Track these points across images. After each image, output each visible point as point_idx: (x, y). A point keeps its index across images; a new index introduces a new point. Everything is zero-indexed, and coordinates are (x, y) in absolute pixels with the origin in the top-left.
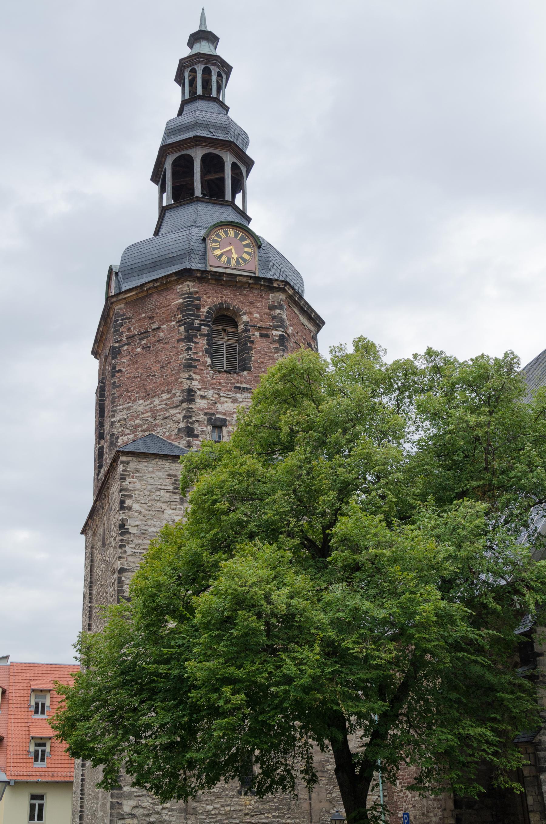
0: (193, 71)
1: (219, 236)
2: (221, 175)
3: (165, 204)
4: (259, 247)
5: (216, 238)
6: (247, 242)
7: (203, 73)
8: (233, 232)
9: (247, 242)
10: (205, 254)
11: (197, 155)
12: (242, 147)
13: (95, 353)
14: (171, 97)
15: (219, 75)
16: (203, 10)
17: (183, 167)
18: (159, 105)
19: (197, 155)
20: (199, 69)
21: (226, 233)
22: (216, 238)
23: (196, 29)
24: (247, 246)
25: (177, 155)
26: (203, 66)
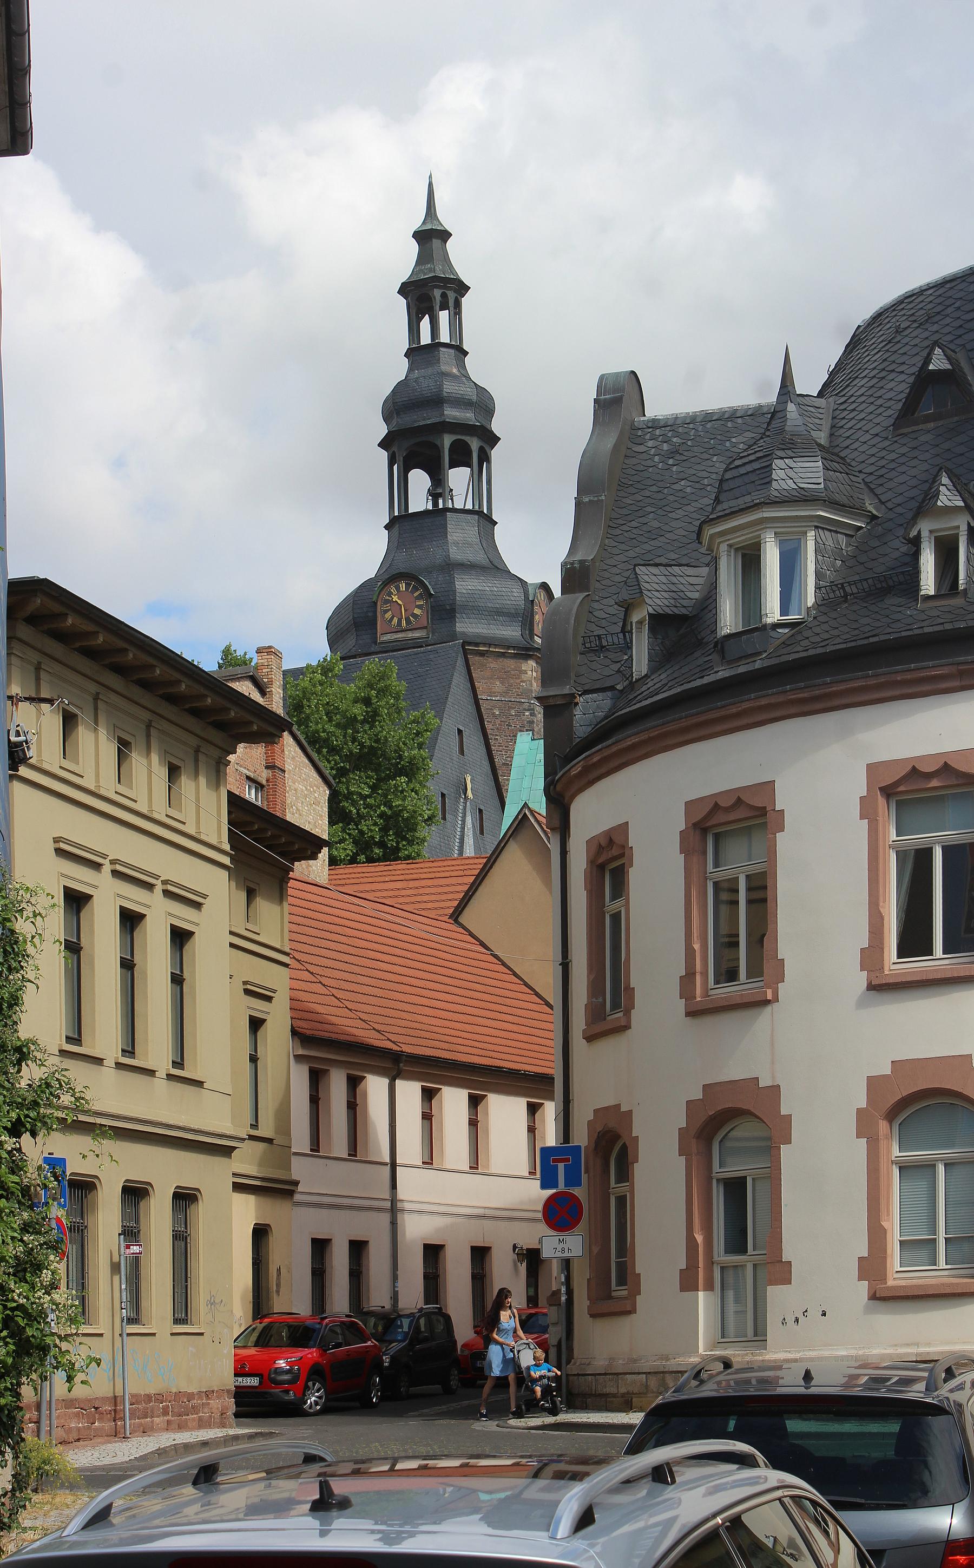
7: (431, 237)
16: (430, 177)
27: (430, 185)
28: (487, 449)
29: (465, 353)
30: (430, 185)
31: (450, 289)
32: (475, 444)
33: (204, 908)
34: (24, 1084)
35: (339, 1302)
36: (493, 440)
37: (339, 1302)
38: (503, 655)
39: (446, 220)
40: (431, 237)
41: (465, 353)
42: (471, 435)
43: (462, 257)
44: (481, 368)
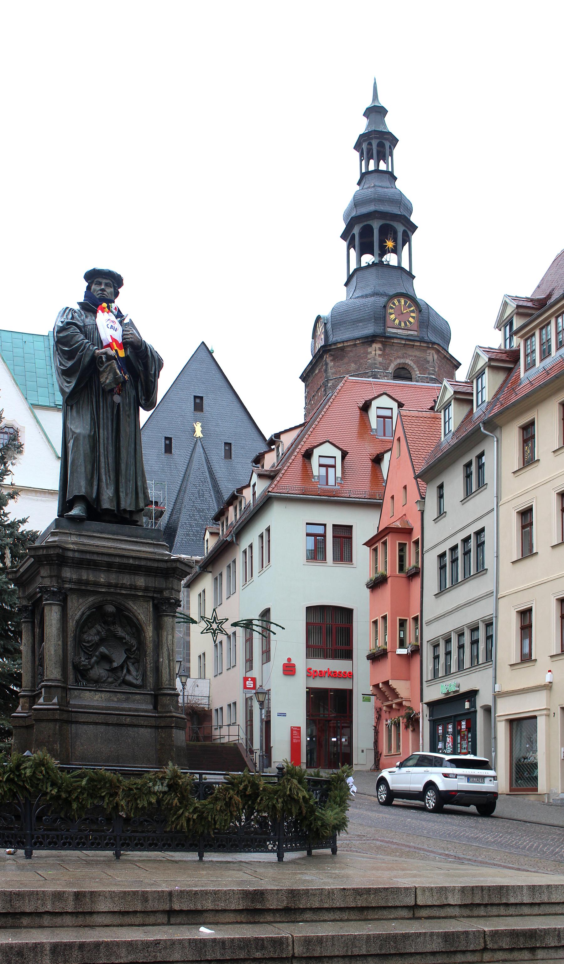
0: (370, 144)
1: (394, 304)
2: (348, 648)
3: (363, 171)
4: (420, 311)
5: (392, 306)
6: (412, 309)
7: (376, 112)
8: (403, 301)
9: (412, 309)
10: (385, 317)
11: (376, 225)
12: (409, 217)
13: (305, 377)
14: (352, 165)
15: (390, 148)
16: (375, 79)
17: (367, 232)
18: (341, 182)
19: (376, 225)
20: (375, 143)
21: (399, 302)
22: (392, 306)
23: (368, 103)
24: (413, 311)
25: (361, 225)
26: (378, 141)
27: (375, 83)
28: (409, 233)
29: (414, 277)
30: (375, 83)
31: (386, 139)
32: (400, 229)
33: (317, 568)
34: (20, 531)
35: (508, 347)
36: (414, 228)
37: (508, 347)
38: (355, 345)
39: (383, 102)
40: (376, 112)
41: (414, 277)
42: (398, 221)
43: (392, 124)
44: (404, 185)
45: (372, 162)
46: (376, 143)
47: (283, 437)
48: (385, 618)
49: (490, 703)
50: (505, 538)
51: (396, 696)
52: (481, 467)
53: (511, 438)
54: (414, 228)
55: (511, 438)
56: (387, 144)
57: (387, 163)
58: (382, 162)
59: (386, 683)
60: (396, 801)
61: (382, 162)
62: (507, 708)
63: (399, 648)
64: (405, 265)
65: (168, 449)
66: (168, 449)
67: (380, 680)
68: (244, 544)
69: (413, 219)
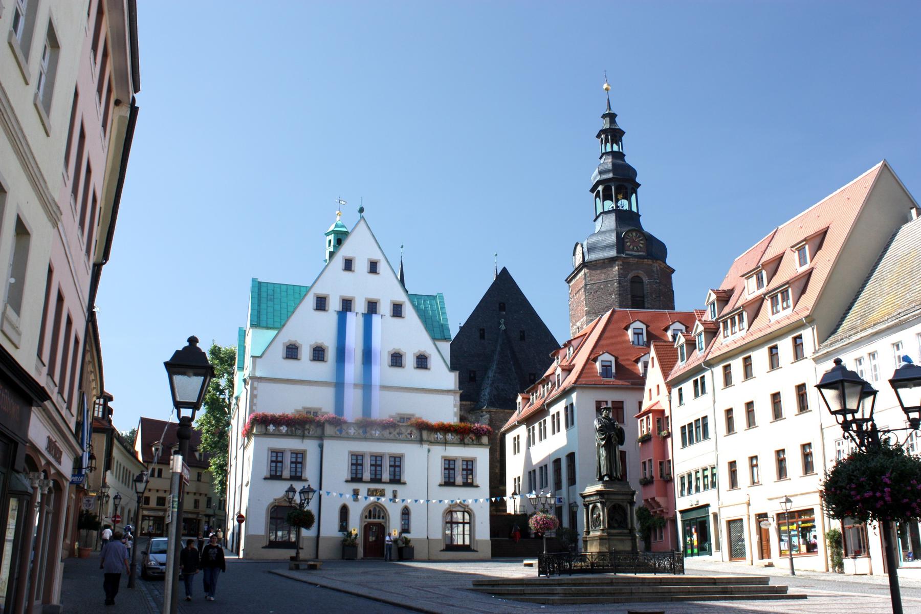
18: (594, 166)
32: (629, 186)
36: (639, 185)
40: (612, 117)
43: (621, 123)
45: (609, 145)
46: (614, 134)
47: (573, 343)
48: (650, 460)
49: (717, 511)
50: (717, 424)
51: (659, 506)
52: (703, 384)
53: (719, 370)
54: (639, 185)
55: (719, 370)
56: (618, 135)
57: (618, 145)
58: (615, 145)
59: (653, 499)
60: (756, 480)
61: (615, 145)
62: (726, 516)
63: (905, 560)
64: (634, 209)
65: (482, 336)
66: (482, 336)
67: (649, 497)
68: (553, 410)
69: (638, 180)
